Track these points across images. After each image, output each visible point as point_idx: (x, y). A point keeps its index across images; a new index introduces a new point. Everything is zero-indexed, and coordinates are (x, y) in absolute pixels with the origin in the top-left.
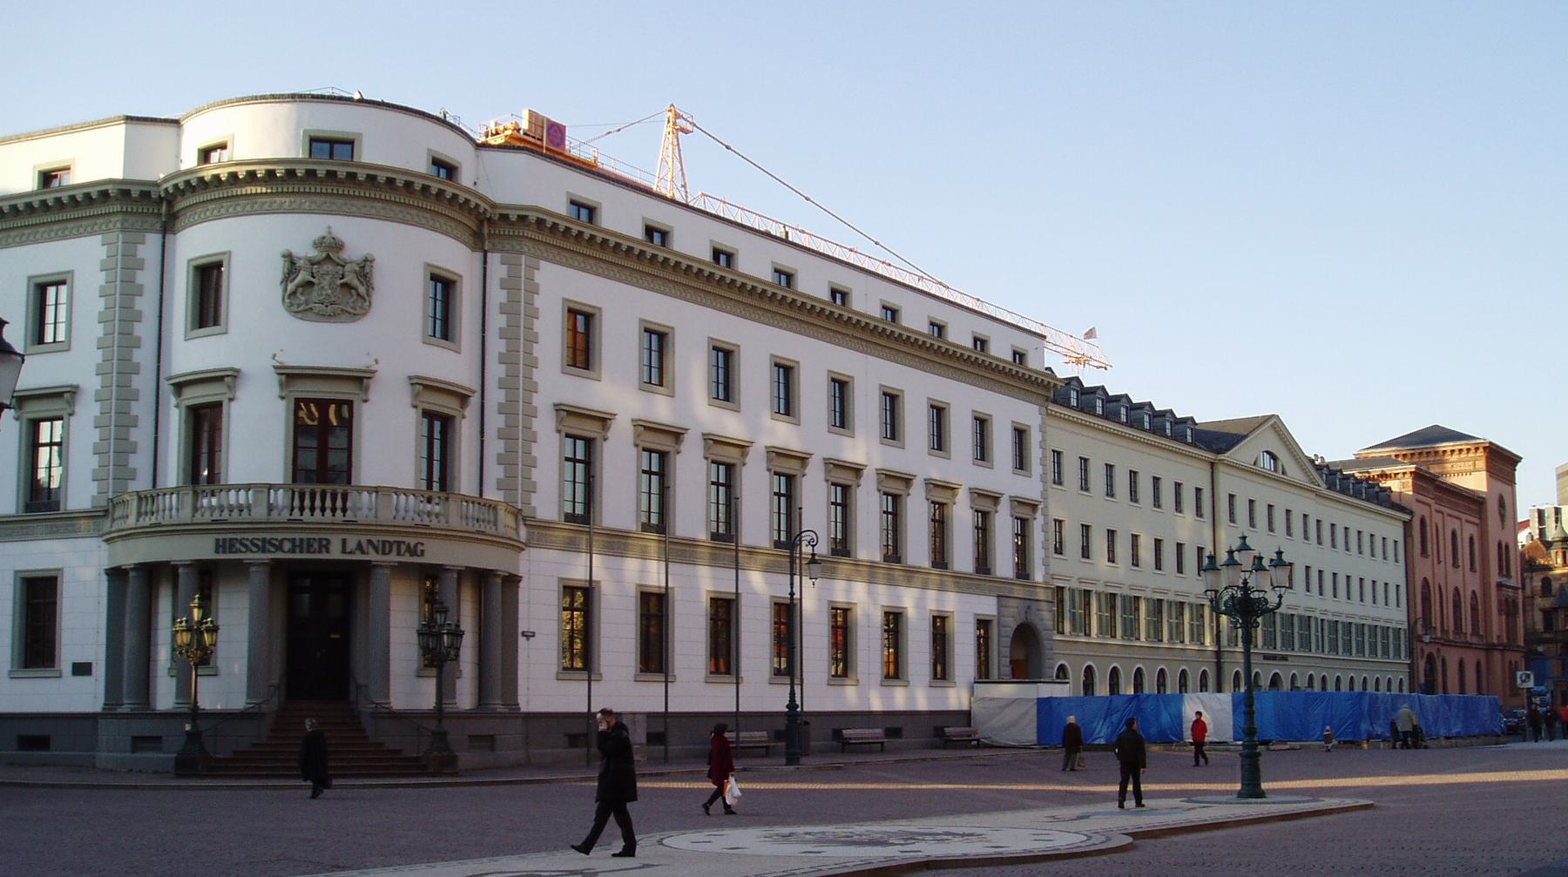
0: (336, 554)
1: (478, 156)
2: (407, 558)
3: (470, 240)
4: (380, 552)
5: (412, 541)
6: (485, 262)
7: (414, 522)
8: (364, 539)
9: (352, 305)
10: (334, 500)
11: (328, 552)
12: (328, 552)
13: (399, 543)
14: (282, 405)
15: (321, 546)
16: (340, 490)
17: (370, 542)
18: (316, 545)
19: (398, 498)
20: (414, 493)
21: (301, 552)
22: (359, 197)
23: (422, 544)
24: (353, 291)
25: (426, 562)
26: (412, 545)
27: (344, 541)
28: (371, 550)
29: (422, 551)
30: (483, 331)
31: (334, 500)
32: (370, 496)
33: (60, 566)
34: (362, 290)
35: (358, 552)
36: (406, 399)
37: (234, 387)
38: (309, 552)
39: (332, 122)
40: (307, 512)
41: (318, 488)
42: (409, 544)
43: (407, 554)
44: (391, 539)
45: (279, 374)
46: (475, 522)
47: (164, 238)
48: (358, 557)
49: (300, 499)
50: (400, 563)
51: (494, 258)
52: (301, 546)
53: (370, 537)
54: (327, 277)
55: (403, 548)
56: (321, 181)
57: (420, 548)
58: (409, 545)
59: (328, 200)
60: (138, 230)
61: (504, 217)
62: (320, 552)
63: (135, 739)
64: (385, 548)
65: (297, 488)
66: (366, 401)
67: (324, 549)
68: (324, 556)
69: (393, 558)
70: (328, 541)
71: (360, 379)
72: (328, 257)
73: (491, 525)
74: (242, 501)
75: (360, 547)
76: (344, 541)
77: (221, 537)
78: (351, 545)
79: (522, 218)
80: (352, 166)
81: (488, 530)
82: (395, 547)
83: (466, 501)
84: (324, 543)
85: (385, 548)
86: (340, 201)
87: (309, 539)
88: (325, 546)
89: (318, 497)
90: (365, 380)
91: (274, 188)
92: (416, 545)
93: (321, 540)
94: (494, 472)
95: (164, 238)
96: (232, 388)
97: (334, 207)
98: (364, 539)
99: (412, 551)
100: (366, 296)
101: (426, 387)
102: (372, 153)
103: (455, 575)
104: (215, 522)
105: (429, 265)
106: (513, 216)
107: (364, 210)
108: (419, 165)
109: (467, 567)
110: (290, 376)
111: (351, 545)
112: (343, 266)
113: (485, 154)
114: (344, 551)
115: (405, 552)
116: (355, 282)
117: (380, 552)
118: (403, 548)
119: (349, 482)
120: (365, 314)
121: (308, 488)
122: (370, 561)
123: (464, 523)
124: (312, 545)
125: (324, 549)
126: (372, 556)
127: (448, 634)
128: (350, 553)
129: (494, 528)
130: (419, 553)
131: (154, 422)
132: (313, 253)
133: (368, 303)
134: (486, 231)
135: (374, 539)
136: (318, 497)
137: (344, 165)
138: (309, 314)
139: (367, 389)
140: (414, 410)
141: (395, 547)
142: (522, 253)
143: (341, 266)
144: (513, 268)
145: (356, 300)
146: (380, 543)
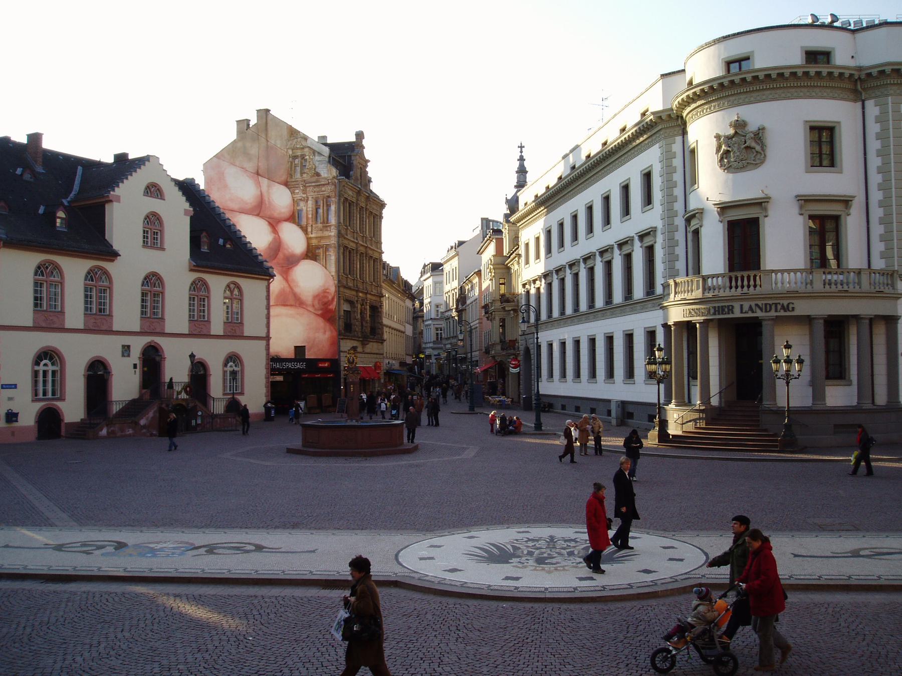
0: (737, 314)
1: (855, 38)
2: (782, 313)
3: (851, 97)
4: (764, 311)
5: (785, 303)
6: (863, 108)
7: (837, 289)
8: (753, 304)
9: (753, 158)
10: (749, 281)
11: (733, 313)
12: (733, 313)
13: (776, 304)
14: (721, 225)
15: (729, 310)
16: (752, 273)
17: (757, 305)
18: (726, 310)
19: (782, 276)
20: (723, 275)
21: (719, 314)
22: (780, 88)
23: (793, 303)
24: (753, 150)
25: (150, 337)
26: (785, 305)
27: (742, 306)
28: (758, 310)
29: (793, 308)
30: (865, 154)
31: (749, 281)
32: (802, 275)
33: (632, 328)
34: (758, 148)
35: (750, 312)
36: (795, 210)
37: (702, 218)
38: (723, 314)
39: (736, 49)
40: (752, 288)
41: (745, 274)
42: (783, 304)
43: (782, 311)
44: (770, 302)
45: (798, 200)
46: (885, 286)
47: (683, 138)
48: (750, 315)
49: (731, 281)
50: (777, 316)
51: (870, 104)
52: (719, 311)
53: (757, 302)
54: (736, 145)
55: (779, 307)
56: (762, 81)
57: (791, 306)
58: (783, 306)
59: (760, 93)
60: (672, 136)
61: (869, 75)
62: (729, 313)
63: (836, 426)
64: (767, 308)
65: (733, 274)
66: (766, 216)
67: (730, 312)
68: (731, 316)
69: (773, 314)
70: (733, 306)
71: (761, 204)
72: (736, 133)
73: (889, 286)
74: (715, 283)
75: (751, 308)
76: (742, 306)
77: (717, 305)
78: (746, 308)
79: (882, 72)
80: (742, 74)
81: (886, 291)
82: (773, 307)
83: (874, 273)
84: (731, 308)
85: (767, 308)
86: (743, 96)
87: (722, 306)
88: (731, 309)
89: (752, 278)
90: (763, 204)
91: (727, 92)
92: (789, 304)
93: (728, 306)
94: (878, 247)
95: (683, 138)
96: (701, 219)
97: (741, 101)
98: (753, 304)
99: (786, 309)
100: (761, 151)
101: (806, 201)
102: (761, 62)
103: (867, 321)
104: (840, 291)
105: (807, 121)
106: (874, 72)
107: (771, 96)
108: (796, 59)
109: (875, 316)
110: (805, 201)
111: (746, 308)
112: (745, 136)
113: (860, 35)
114: (742, 312)
115: (781, 309)
116: (753, 144)
117: (764, 311)
118: (779, 307)
119: (759, 268)
120: (762, 163)
121: (739, 274)
122: (758, 317)
123: (873, 287)
124: (724, 310)
125: (730, 312)
126: (759, 314)
127: (774, 363)
128: (745, 313)
129: (891, 288)
130: (790, 309)
131: (685, 242)
132: (731, 131)
133: (763, 156)
134: (859, 87)
135: (760, 303)
136: (752, 278)
137: (737, 74)
138: (731, 170)
139: (766, 209)
140: (802, 216)
141: (773, 307)
142: (887, 95)
143: (743, 136)
144: (883, 106)
145: (756, 155)
146: (764, 306)
